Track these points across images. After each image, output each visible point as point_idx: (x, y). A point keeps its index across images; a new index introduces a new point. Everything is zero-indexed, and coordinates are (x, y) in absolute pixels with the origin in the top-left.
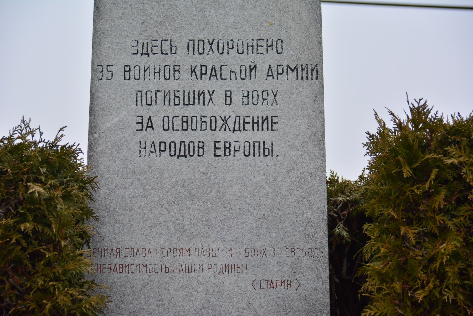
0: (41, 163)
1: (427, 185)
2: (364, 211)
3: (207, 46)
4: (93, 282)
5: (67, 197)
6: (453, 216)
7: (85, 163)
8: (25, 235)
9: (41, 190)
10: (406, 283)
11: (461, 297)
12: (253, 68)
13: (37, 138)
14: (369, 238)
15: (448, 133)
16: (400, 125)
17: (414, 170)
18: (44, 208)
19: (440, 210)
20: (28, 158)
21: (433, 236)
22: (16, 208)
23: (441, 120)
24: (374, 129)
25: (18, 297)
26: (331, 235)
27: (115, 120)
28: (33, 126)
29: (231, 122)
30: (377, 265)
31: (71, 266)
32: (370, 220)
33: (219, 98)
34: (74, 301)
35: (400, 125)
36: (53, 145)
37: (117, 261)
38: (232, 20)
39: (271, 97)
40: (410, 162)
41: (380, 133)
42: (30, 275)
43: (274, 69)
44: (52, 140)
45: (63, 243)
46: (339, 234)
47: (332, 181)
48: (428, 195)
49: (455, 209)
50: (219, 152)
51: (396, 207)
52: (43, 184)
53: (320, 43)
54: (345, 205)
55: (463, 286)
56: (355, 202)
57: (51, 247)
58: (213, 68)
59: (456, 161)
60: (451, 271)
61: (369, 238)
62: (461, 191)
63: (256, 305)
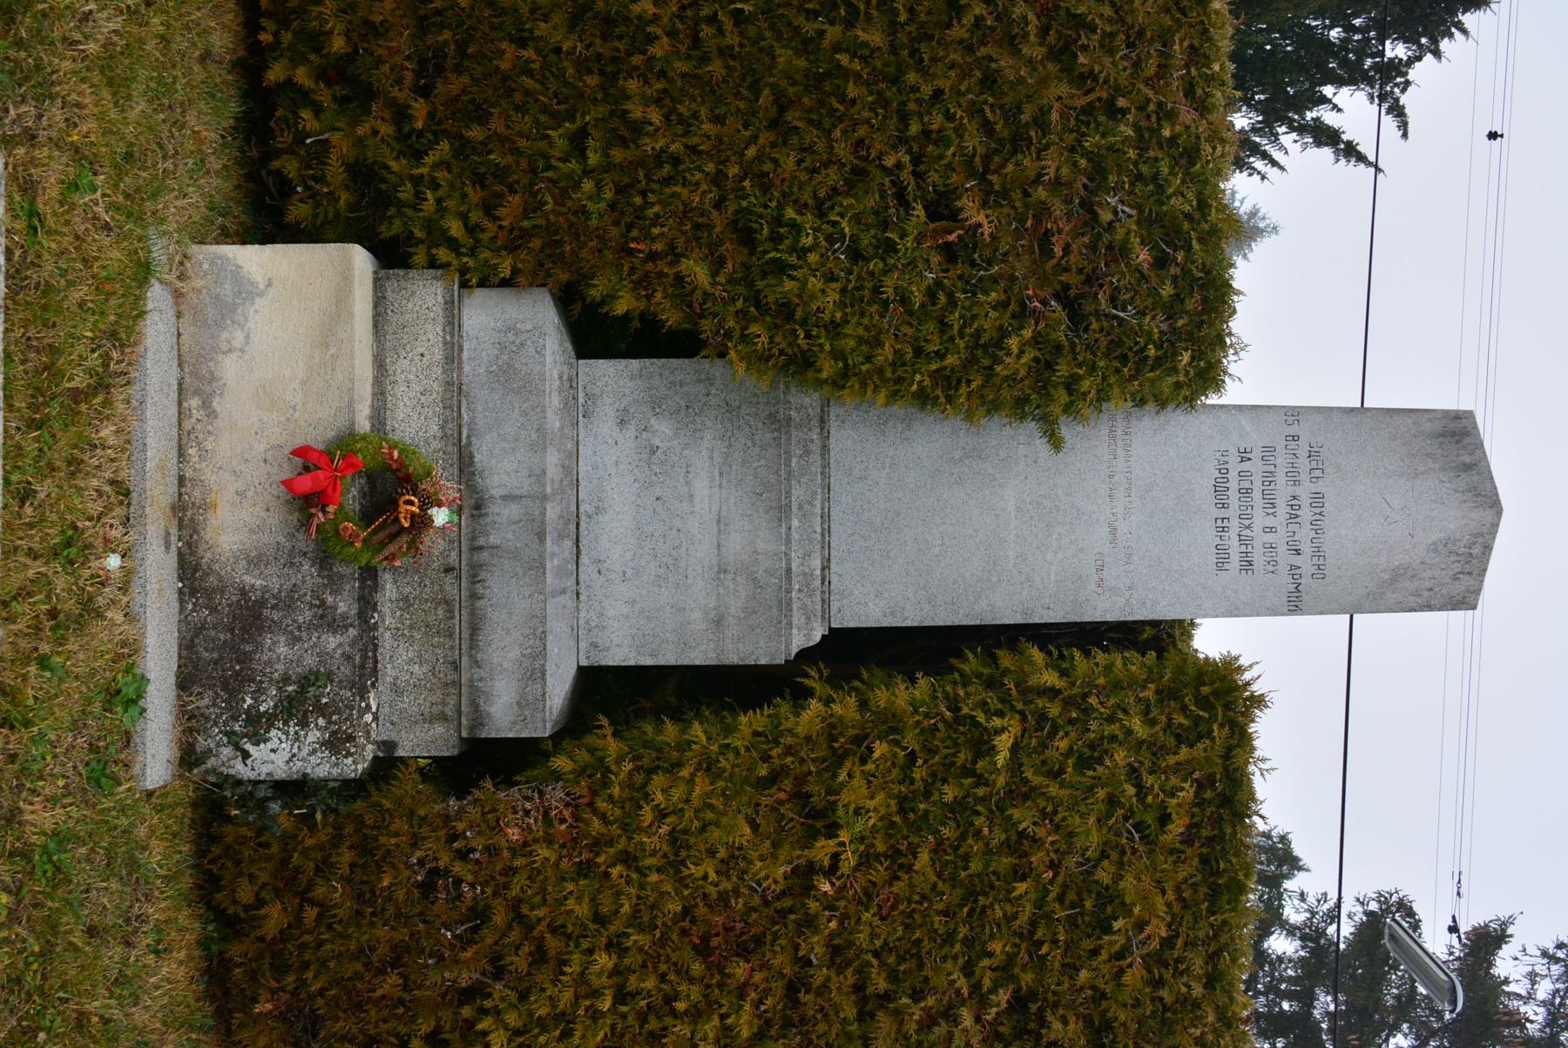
0: (1209, 362)
1: (1194, 708)
2: (1168, 652)
3: (1318, 510)
4: (1101, 411)
5: (1178, 385)
6: (1165, 731)
7: (1209, 402)
8: (1143, 349)
9: (1184, 362)
10: (1104, 688)
11: (1093, 736)
12: (1298, 552)
13: (1231, 358)
14: (1143, 656)
15: (1242, 728)
16: (1248, 684)
17: (1207, 697)
18: (1168, 365)
19: (1170, 720)
20: (1213, 350)
21: (1147, 713)
22: (1168, 340)
23: (1253, 721)
24: (1243, 661)
25: (1088, 345)
26: (1143, 623)
27: (1248, 429)
28: (1242, 354)
29: (1247, 532)
30: (1119, 663)
31: (1116, 390)
32: (1160, 657)
33: (1270, 521)
34: (1085, 394)
35: (1248, 684)
36: (1225, 372)
37: (1119, 432)
38: (1344, 532)
39: (1272, 569)
40: (1215, 693)
41: (1240, 667)
42: (1107, 355)
43: (1298, 571)
44: (1230, 371)
45: (1136, 383)
46: (1144, 631)
47: (1192, 624)
48: (1184, 709)
49: (1172, 733)
50: (1219, 521)
51: (1173, 680)
52: (1190, 364)
53: (1322, 613)
54: (1171, 636)
55: (1102, 738)
56: (1175, 645)
57: (1133, 372)
58: (1297, 516)
59: (1215, 734)
60: (1115, 728)
61: (1143, 656)
62: (1188, 738)
63: (1081, 556)
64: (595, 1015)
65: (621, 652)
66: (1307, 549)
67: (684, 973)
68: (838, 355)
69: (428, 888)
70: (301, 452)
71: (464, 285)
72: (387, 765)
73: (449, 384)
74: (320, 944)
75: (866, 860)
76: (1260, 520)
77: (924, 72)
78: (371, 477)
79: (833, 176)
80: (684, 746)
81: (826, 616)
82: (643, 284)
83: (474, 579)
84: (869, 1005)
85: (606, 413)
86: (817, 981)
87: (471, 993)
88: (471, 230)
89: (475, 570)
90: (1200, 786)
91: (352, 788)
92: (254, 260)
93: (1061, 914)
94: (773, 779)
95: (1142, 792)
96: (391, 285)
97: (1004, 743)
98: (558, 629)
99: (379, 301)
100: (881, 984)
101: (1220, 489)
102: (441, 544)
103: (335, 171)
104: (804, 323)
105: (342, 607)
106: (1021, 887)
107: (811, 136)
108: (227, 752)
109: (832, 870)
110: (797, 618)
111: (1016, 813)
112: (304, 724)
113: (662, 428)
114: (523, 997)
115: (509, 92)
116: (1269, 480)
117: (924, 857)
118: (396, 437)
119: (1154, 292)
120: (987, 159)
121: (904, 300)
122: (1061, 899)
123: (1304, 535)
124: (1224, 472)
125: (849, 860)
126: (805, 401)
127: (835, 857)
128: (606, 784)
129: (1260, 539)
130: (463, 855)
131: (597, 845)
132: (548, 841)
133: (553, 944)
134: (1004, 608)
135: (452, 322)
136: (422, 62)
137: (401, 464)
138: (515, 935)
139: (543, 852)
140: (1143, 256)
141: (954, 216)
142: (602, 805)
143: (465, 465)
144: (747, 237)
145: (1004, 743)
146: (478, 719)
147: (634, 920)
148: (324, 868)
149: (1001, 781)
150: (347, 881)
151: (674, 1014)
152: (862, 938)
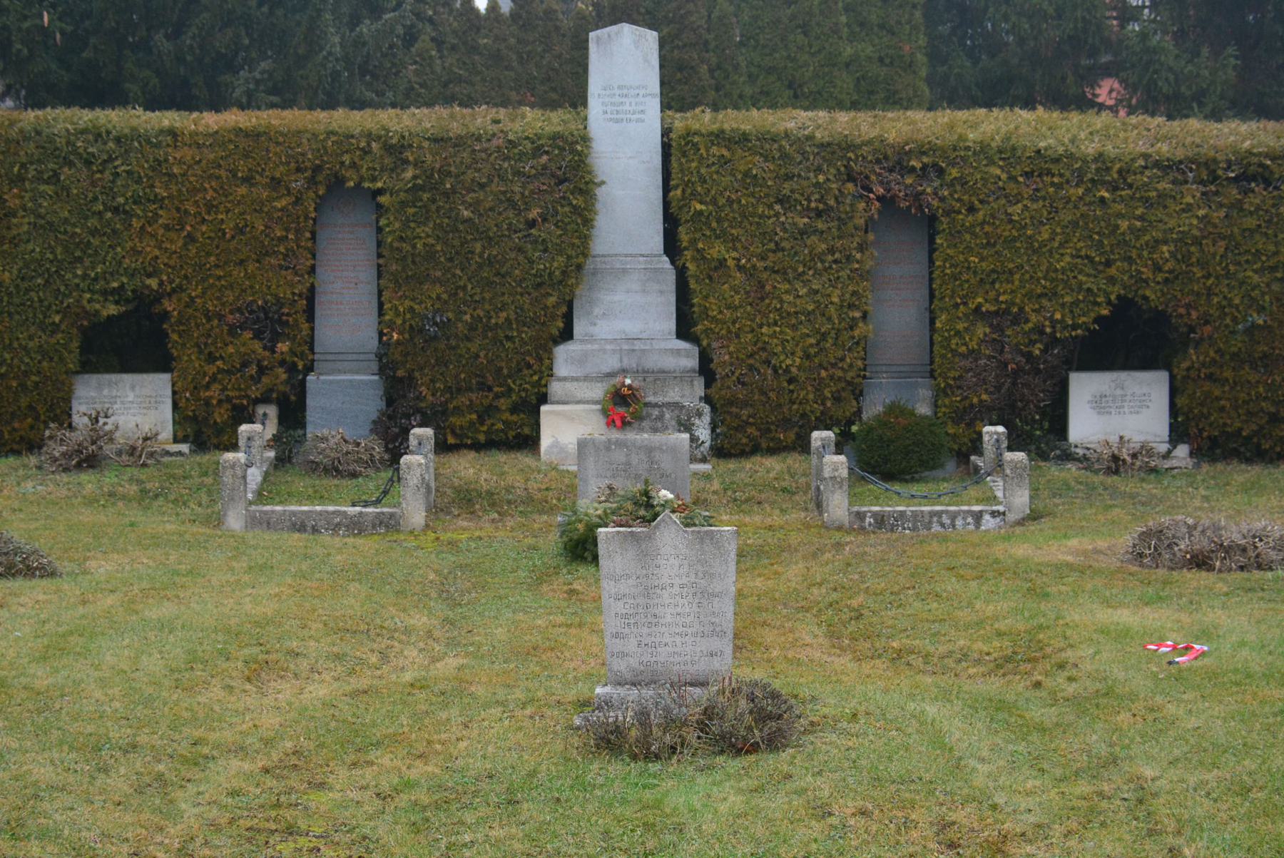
33: (633, 104)
64: (781, 332)
65: (672, 325)
66: (637, 92)
67: (769, 305)
68: (577, 257)
69: (743, 384)
70: (608, 424)
71: (552, 376)
72: (707, 399)
73: (585, 380)
74: (761, 418)
75: (735, 249)
76: (627, 107)
77: (489, 229)
78: (615, 404)
79: (521, 258)
80: (700, 305)
81: (660, 256)
82: (553, 317)
83: (648, 372)
84: (778, 248)
85: (592, 330)
86: (771, 264)
87: (775, 370)
88: (535, 373)
89: (644, 372)
90: (713, 144)
91: (714, 409)
92: (545, 442)
93: (752, 189)
94: (710, 278)
95: (713, 164)
96: (553, 399)
97: (699, 207)
98: (663, 345)
99: (558, 403)
100: (772, 246)
101: (617, 121)
102: (636, 382)
103: (515, 418)
104: (567, 267)
105: (657, 413)
106: (743, 202)
107: (508, 265)
108: (702, 449)
109: (739, 260)
110: (660, 266)
111: (720, 204)
112: (693, 425)
113: (597, 311)
114: (776, 354)
115: (493, 360)
116: (613, 104)
117: (734, 231)
118: (602, 397)
119: (556, 155)
120: (515, 209)
121: (561, 236)
122: (747, 189)
123: (632, 92)
124: (611, 119)
125: (735, 254)
126: (589, 265)
127: (734, 259)
128: (711, 329)
129: (634, 107)
130: (733, 373)
131: (729, 332)
132: (728, 347)
133: (760, 345)
134: (658, 194)
135: (565, 379)
136: (480, 389)
137: (612, 393)
138: (757, 357)
139: (731, 349)
140: (545, 157)
141: (534, 221)
142: (717, 330)
143: (611, 375)
144: (540, 285)
145: (699, 207)
146: (693, 371)
147: (752, 320)
148: (737, 416)
149: (711, 208)
150: (741, 409)
151: (781, 308)
152: (759, 251)
